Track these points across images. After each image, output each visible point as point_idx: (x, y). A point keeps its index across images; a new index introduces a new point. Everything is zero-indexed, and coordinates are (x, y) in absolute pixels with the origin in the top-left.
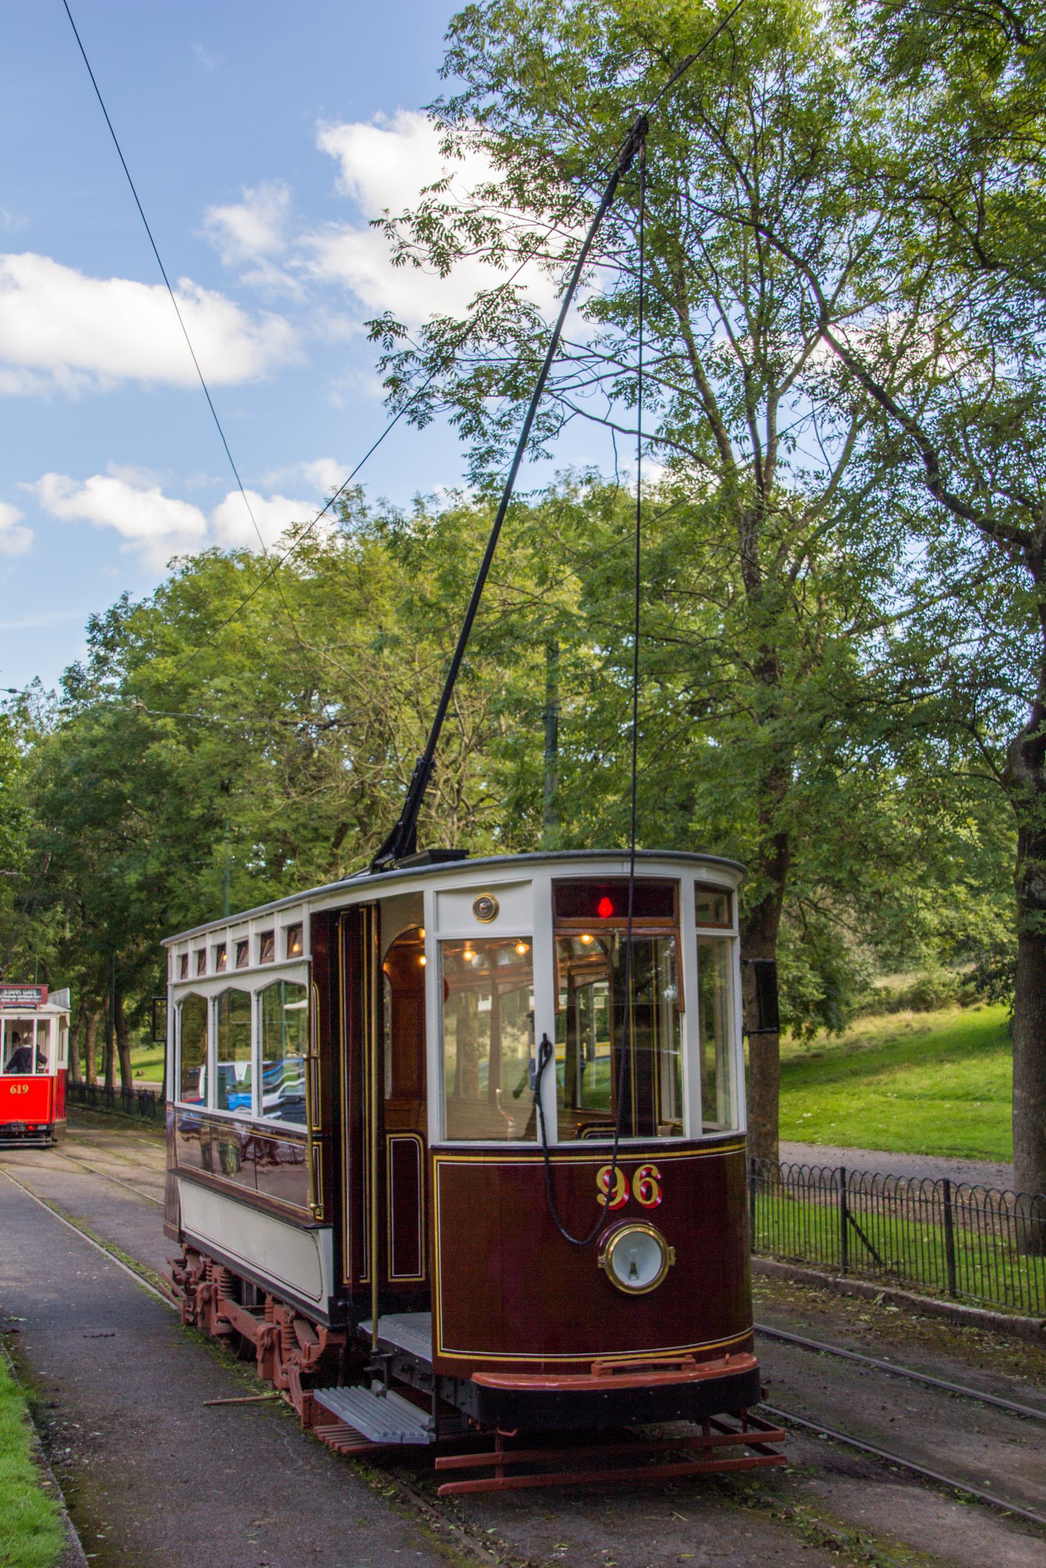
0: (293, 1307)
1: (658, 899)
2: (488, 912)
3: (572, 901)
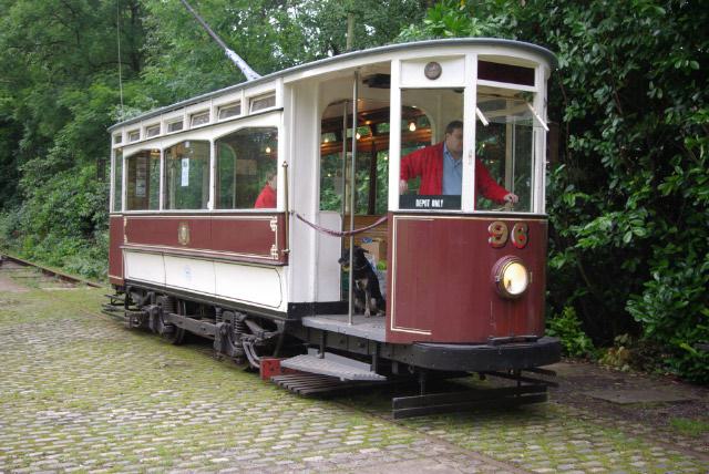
0: (245, 313)
1: (526, 76)
2: (433, 70)
3: (487, 70)
